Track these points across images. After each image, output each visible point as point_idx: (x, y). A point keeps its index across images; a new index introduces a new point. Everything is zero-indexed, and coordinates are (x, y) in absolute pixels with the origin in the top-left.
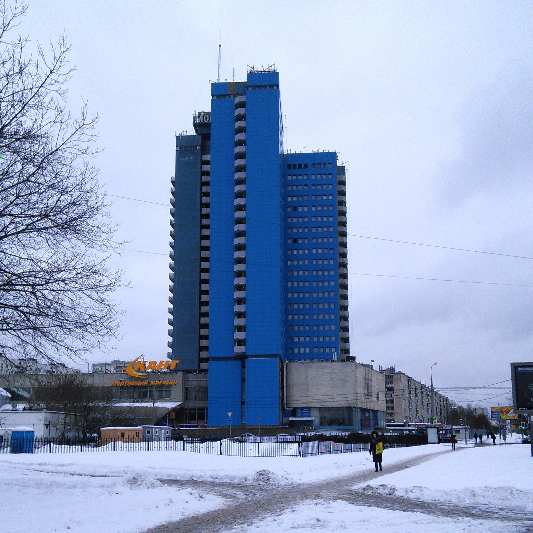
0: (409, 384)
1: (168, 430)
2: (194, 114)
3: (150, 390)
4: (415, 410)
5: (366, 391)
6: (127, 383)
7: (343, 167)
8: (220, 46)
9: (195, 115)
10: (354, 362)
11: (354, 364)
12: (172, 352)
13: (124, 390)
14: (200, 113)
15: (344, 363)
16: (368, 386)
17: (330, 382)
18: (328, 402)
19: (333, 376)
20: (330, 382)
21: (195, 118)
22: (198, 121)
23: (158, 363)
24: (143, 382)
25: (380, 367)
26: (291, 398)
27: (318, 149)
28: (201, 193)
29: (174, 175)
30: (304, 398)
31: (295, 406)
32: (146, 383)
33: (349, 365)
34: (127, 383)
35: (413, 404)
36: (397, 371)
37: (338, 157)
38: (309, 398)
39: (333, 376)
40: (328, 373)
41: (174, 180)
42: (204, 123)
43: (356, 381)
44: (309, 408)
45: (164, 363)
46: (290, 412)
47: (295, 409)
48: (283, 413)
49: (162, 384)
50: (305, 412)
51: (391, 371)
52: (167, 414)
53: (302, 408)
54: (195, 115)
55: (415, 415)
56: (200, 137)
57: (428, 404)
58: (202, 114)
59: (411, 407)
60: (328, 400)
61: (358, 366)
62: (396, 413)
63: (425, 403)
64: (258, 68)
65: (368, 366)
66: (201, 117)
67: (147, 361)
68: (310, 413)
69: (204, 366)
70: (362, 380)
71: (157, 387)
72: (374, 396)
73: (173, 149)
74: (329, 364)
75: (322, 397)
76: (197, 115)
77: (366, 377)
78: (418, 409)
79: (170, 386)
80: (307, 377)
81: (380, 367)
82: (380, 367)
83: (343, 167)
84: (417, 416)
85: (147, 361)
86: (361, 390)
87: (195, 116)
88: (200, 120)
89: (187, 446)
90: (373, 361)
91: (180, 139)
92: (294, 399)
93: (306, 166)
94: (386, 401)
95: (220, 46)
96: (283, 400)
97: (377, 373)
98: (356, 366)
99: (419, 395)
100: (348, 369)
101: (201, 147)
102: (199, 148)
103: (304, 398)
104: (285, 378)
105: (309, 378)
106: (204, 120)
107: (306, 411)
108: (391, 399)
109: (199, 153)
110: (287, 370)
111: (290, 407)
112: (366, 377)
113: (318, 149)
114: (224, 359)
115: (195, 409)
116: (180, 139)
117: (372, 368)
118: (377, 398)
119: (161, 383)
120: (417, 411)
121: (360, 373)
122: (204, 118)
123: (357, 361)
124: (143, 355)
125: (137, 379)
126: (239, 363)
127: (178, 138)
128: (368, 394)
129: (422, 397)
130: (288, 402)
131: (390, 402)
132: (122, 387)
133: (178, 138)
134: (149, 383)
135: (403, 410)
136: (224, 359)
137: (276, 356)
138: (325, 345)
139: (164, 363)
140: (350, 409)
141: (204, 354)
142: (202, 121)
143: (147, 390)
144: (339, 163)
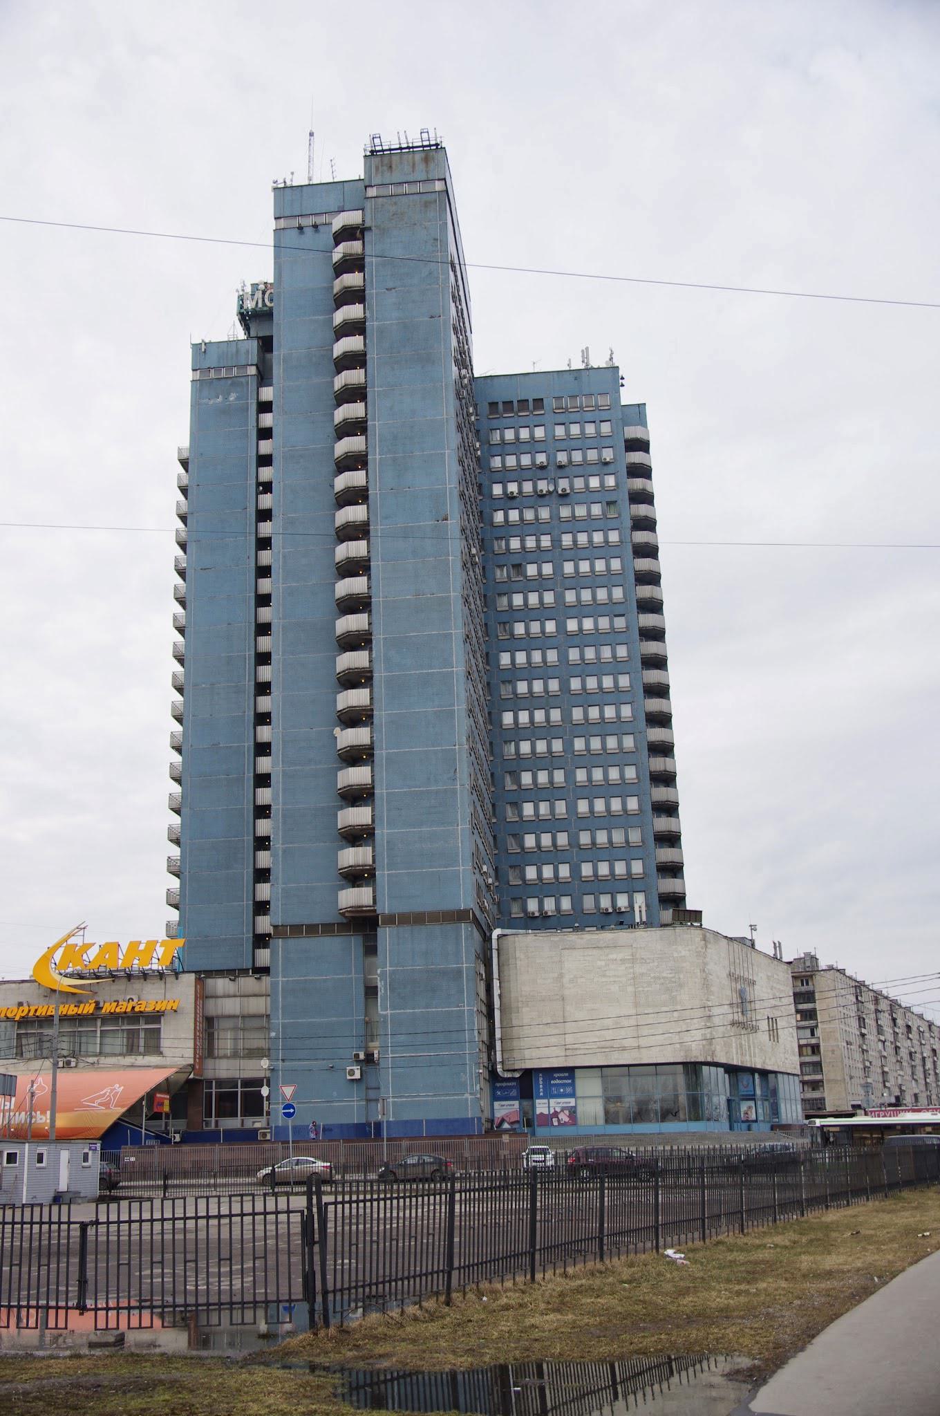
0: (857, 999)
1: (86, 1150)
2: (240, 289)
3: (103, 1029)
4: (879, 1071)
5: (738, 1017)
6: (36, 1011)
7: (641, 407)
8: (311, 134)
9: (243, 290)
10: (697, 927)
11: (698, 932)
12: (178, 919)
13: (29, 1032)
14: (255, 286)
15: (668, 932)
16: (743, 1002)
17: (630, 989)
18: (624, 1049)
19: (639, 969)
20: (630, 989)
21: (241, 299)
22: (250, 305)
23: (124, 948)
24: (82, 1006)
25: (777, 946)
26: (515, 1043)
27: (570, 360)
28: (258, 484)
29: (185, 442)
30: (553, 1040)
31: (529, 1065)
32: (88, 1008)
33: (686, 935)
34: (36, 1011)
35: (873, 1054)
36: (823, 964)
37: (622, 378)
38: (569, 1039)
39: (639, 969)
40: (623, 961)
41: (185, 455)
42: (265, 309)
43: (706, 984)
44: (570, 1071)
45: (142, 947)
46: (514, 1084)
47: (528, 1074)
48: (494, 1089)
49: (137, 1009)
50: (558, 1081)
51: (808, 964)
52: (142, 1099)
53: (549, 1072)
54: (243, 290)
55: (881, 1085)
56: (255, 343)
57: (911, 1054)
58: (262, 287)
59: (867, 1064)
60: (627, 1043)
61: (712, 940)
62: (829, 1081)
63: (904, 1053)
64: (390, 141)
65: (742, 940)
66: (259, 295)
67: (94, 944)
68: (573, 1085)
69: (264, 957)
70: (726, 982)
71: (123, 1018)
72: (764, 1025)
73: (182, 378)
74: (623, 936)
75: (609, 1035)
76: (249, 289)
77: (737, 973)
78: (886, 1069)
79: (156, 1017)
80: (561, 976)
81: (774, 943)
82: (777, 946)
83: (641, 407)
84: (885, 1086)
85: (94, 944)
86: (723, 1014)
87: (241, 293)
88: (254, 303)
89: (794, 1114)
90: (753, 928)
91: (201, 351)
92: (524, 1043)
93: (539, 403)
94: (800, 1047)
95: (311, 134)
96: (491, 1047)
97: (767, 961)
98: (705, 940)
99: (888, 1030)
100: (680, 948)
101: (257, 368)
102: (252, 371)
103: (553, 1040)
104: (496, 983)
105: (566, 980)
106: (266, 300)
107: (560, 1078)
108: (813, 1041)
109: (253, 383)
110: (502, 958)
111: (514, 1070)
112: (737, 973)
113: (570, 360)
114: (312, 930)
115: (232, 1082)
116: (201, 351)
117: (753, 946)
118: (773, 1032)
119: (133, 1008)
120: (884, 1073)
121: (719, 963)
122: (266, 296)
123: (706, 922)
124: (82, 926)
125: (68, 996)
126: (355, 943)
127: (196, 347)
128: (744, 1026)
129: (896, 1034)
130: (506, 1056)
131: (809, 1049)
132: (24, 1022)
133: (196, 347)
134: (98, 1007)
135: (847, 1070)
136: (312, 930)
137: (460, 916)
138: (611, 885)
139: (142, 947)
140: (692, 1069)
141: (264, 924)
142: (260, 305)
143: (142, 1035)
144: (628, 397)
